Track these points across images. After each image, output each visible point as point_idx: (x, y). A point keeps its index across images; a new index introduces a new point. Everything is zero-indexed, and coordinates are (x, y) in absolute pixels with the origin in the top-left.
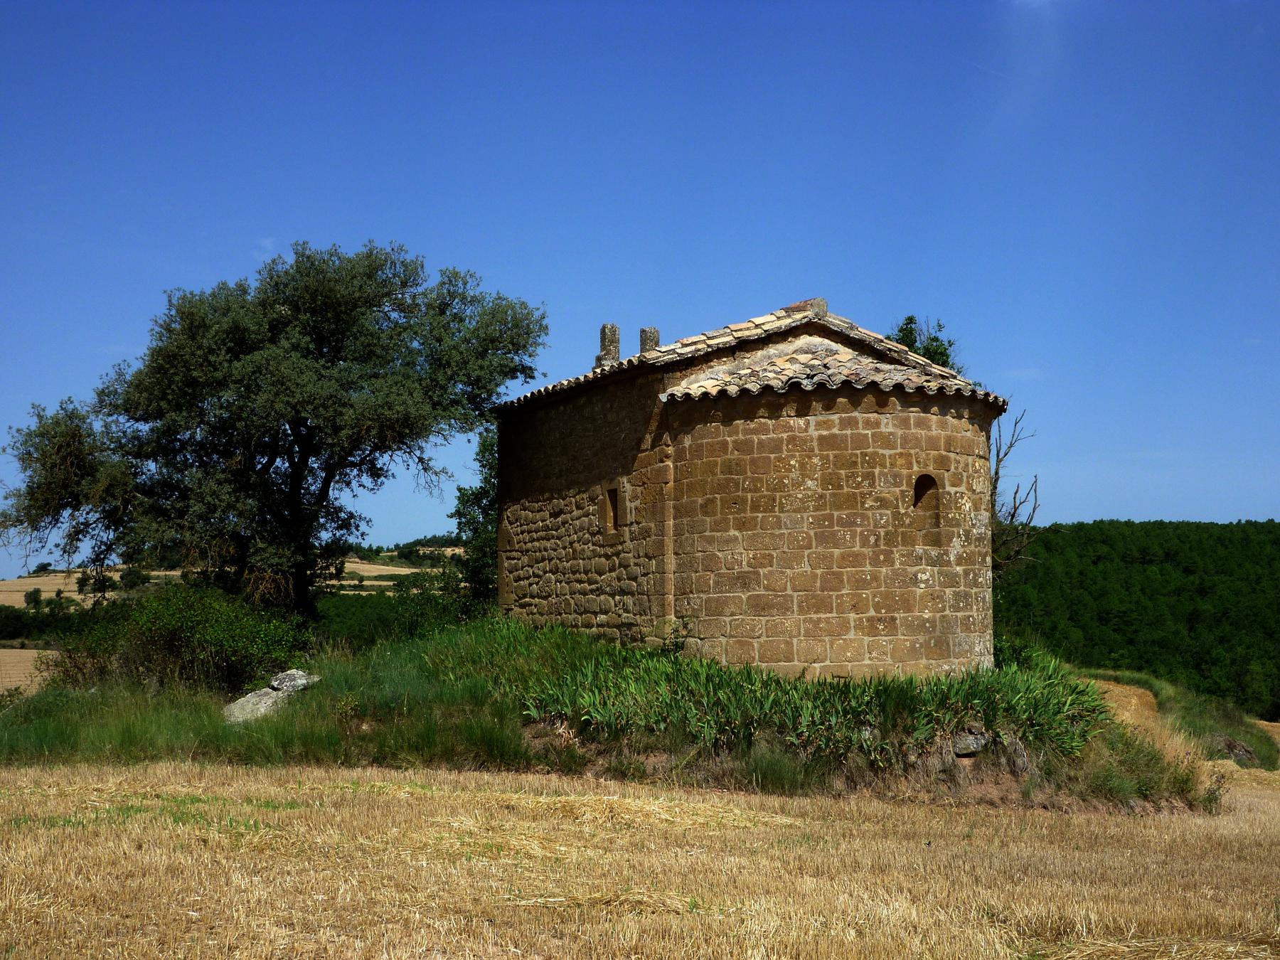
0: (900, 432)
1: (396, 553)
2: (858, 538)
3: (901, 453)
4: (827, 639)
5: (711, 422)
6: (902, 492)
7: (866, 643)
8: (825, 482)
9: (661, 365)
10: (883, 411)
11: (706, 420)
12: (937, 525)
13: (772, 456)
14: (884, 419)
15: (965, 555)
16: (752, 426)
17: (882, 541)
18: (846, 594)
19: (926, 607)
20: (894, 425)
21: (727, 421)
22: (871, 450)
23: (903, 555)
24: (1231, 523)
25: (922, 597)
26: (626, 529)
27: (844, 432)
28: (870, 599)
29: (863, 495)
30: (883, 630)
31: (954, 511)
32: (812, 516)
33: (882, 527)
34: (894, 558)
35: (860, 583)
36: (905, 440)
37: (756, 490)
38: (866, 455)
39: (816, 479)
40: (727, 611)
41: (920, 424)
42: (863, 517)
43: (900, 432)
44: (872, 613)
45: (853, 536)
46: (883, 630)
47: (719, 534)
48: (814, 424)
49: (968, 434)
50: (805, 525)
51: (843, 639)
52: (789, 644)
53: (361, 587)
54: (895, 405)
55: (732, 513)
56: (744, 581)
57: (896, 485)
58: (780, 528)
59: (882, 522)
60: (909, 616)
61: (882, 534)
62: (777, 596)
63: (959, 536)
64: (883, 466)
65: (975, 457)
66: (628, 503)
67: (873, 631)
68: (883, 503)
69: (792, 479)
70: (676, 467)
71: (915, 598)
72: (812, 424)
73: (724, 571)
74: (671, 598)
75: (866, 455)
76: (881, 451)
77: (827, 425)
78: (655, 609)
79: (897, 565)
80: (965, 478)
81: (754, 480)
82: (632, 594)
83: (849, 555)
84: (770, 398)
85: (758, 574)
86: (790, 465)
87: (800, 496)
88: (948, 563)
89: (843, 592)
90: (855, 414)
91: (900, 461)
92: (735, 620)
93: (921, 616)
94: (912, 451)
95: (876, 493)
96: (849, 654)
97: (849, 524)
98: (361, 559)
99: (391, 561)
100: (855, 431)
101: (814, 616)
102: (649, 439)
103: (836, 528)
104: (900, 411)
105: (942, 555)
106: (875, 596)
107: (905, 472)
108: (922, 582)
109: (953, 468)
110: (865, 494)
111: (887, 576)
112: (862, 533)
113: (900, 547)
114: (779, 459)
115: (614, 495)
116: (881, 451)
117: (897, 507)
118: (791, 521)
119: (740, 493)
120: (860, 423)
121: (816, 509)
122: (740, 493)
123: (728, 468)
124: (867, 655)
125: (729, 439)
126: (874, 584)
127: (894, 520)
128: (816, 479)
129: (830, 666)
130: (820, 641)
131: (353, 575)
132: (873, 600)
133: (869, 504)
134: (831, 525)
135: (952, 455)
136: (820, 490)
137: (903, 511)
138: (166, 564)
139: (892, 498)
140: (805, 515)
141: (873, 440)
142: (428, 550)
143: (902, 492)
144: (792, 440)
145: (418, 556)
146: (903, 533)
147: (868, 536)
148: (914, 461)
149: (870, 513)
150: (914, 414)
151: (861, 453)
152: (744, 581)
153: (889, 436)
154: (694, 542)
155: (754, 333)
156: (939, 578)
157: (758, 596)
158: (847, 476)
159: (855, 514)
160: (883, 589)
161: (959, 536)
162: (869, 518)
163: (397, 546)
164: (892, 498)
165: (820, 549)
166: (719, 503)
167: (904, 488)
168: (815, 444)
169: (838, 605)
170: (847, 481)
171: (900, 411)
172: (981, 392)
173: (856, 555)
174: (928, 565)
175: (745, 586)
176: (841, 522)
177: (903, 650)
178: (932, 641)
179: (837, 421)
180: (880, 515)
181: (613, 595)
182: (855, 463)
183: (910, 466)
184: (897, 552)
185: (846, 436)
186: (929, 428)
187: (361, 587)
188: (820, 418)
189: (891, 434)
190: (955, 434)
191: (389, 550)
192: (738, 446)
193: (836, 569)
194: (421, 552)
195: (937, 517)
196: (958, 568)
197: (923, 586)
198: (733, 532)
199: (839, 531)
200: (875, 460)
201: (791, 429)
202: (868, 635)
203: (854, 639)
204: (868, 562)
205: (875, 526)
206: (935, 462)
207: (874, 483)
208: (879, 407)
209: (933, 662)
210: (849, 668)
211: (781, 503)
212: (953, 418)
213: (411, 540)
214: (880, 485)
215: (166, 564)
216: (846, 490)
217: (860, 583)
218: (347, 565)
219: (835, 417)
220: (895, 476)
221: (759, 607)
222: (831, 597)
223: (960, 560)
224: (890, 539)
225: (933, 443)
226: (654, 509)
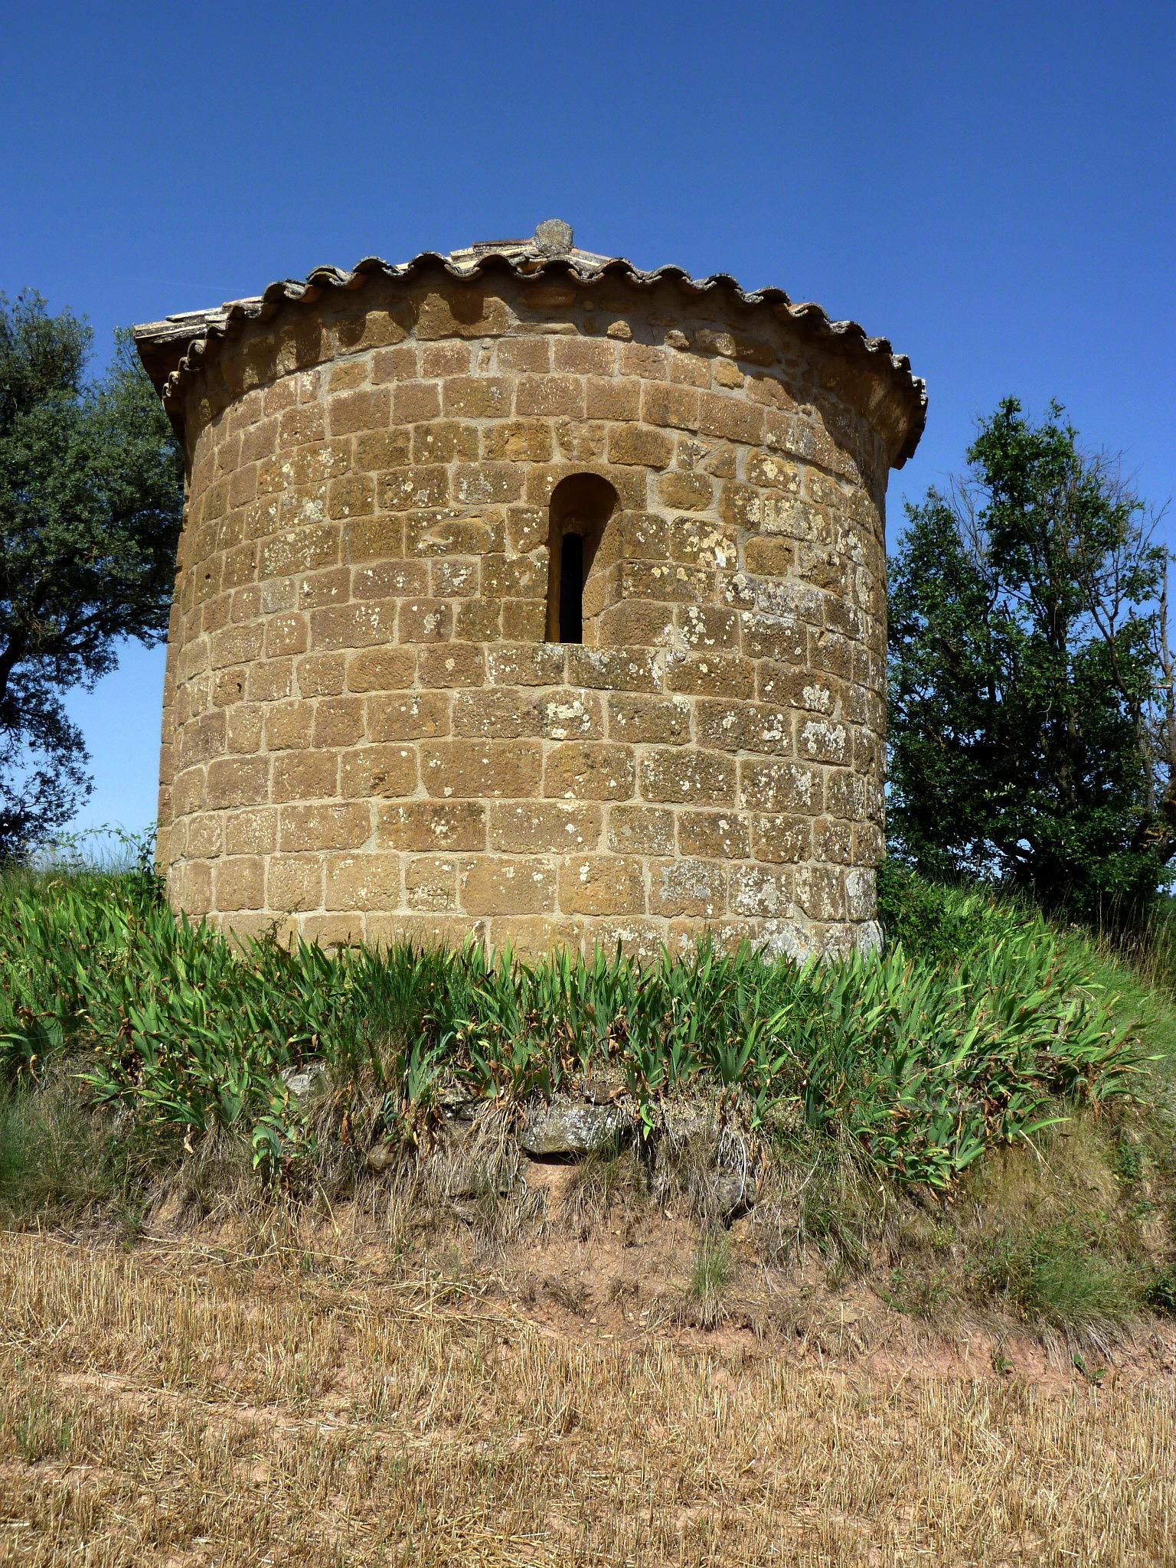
0: (516, 379)
2: (396, 622)
3: (518, 426)
4: (321, 855)
6: (515, 512)
7: (403, 867)
8: (337, 503)
9: (166, 344)
10: (472, 330)
13: (259, 463)
14: (475, 350)
15: (704, 668)
17: (455, 626)
18: (365, 751)
19: (568, 785)
20: (503, 362)
22: (440, 420)
23: (507, 660)
25: (556, 760)
27: (382, 386)
28: (419, 761)
29: (414, 523)
30: (446, 836)
31: (670, 560)
32: (309, 579)
33: (455, 594)
34: (481, 667)
36: (530, 395)
38: (428, 432)
39: (322, 498)
41: (571, 359)
42: (414, 572)
43: (516, 379)
44: (421, 795)
45: (386, 619)
46: (446, 836)
48: (328, 378)
49: (738, 394)
50: (296, 600)
51: (353, 857)
52: (257, 867)
54: (502, 314)
57: (498, 496)
59: (456, 581)
60: (518, 805)
61: (456, 609)
63: (685, 620)
64: (468, 454)
65: (764, 450)
68: (461, 539)
69: (283, 505)
71: (536, 764)
72: (326, 378)
75: (428, 432)
76: (464, 422)
79: (490, 683)
80: (718, 493)
83: (375, 661)
84: (252, 341)
86: (281, 475)
87: (291, 538)
88: (645, 682)
89: (358, 747)
90: (411, 344)
93: (553, 806)
94: (551, 422)
95: (448, 515)
96: (363, 892)
97: (379, 588)
100: (407, 383)
101: (300, 804)
103: (352, 601)
104: (518, 329)
105: (626, 663)
106: (428, 755)
107: (526, 467)
108: (556, 723)
109: (673, 463)
110: (419, 520)
111: (461, 707)
112: (405, 609)
113: (501, 641)
116: (464, 422)
117: (499, 546)
118: (273, 594)
120: (420, 364)
121: (319, 561)
124: (404, 896)
126: (429, 727)
127: (488, 577)
128: (322, 498)
129: (323, 918)
130: (308, 860)
132: (424, 766)
133: (429, 538)
134: (342, 597)
135: (674, 436)
136: (327, 521)
137: (512, 556)
139: (488, 528)
140: (297, 578)
141: (446, 397)
143: (515, 512)
146: (509, 607)
147: (421, 614)
148: (555, 442)
149: (427, 563)
151: (417, 429)
153: (489, 387)
156: (613, 718)
158: (381, 483)
159: (393, 566)
160: (450, 738)
161: (685, 620)
162: (425, 573)
164: (488, 528)
165: (319, 652)
167: (522, 503)
168: (326, 421)
169: (347, 776)
170: (382, 493)
171: (518, 329)
173: (391, 660)
174: (579, 684)
177: (495, 887)
178: (584, 869)
179: (370, 365)
180: (452, 565)
182: (402, 452)
183: (541, 453)
184: (491, 650)
185: (386, 394)
186: (602, 369)
188: (341, 364)
189: (493, 382)
190: (685, 387)
193: (347, 695)
196: (678, 698)
197: (560, 733)
199: (357, 607)
202: (409, 847)
203: (377, 858)
204: (416, 675)
205: (439, 592)
206: (616, 445)
207: (442, 494)
208: (463, 322)
209: (586, 920)
210: (363, 925)
212: (681, 349)
214: (456, 499)
216: (378, 512)
217: (397, 726)
219: (367, 358)
220: (498, 477)
222: (332, 757)
223: (683, 678)
224: (476, 622)
225: (612, 404)
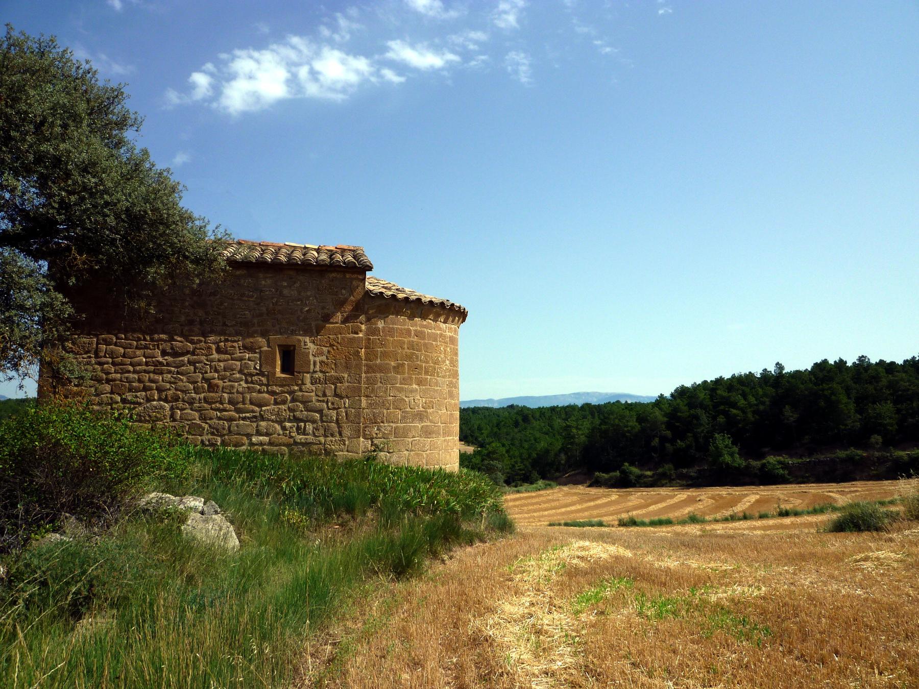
5: (401, 316)
11: (398, 313)
13: (434, 343)
16: (425, 323)
21: (411, 317)
24: (661, 396)
26: (308, 375)
37: (427, 362)
40: (410, 435)
47: (406, 386)
55: (414, 374)
58: (437, 386)
62: (435, 426)
66: (311, 358)
73: (409, 409)
81: (425, 356)
85: (426, 412)
92: (415, 440)
102: (339, 317)
119: (419, 363)
122: (419, 363)
123: (412, 346)
125: (411, 328)
154: (387, 389)
157: (427, 426)
166: (406, 367)
175: (421, 420)
198: (414, 386)
211: (438, 372)
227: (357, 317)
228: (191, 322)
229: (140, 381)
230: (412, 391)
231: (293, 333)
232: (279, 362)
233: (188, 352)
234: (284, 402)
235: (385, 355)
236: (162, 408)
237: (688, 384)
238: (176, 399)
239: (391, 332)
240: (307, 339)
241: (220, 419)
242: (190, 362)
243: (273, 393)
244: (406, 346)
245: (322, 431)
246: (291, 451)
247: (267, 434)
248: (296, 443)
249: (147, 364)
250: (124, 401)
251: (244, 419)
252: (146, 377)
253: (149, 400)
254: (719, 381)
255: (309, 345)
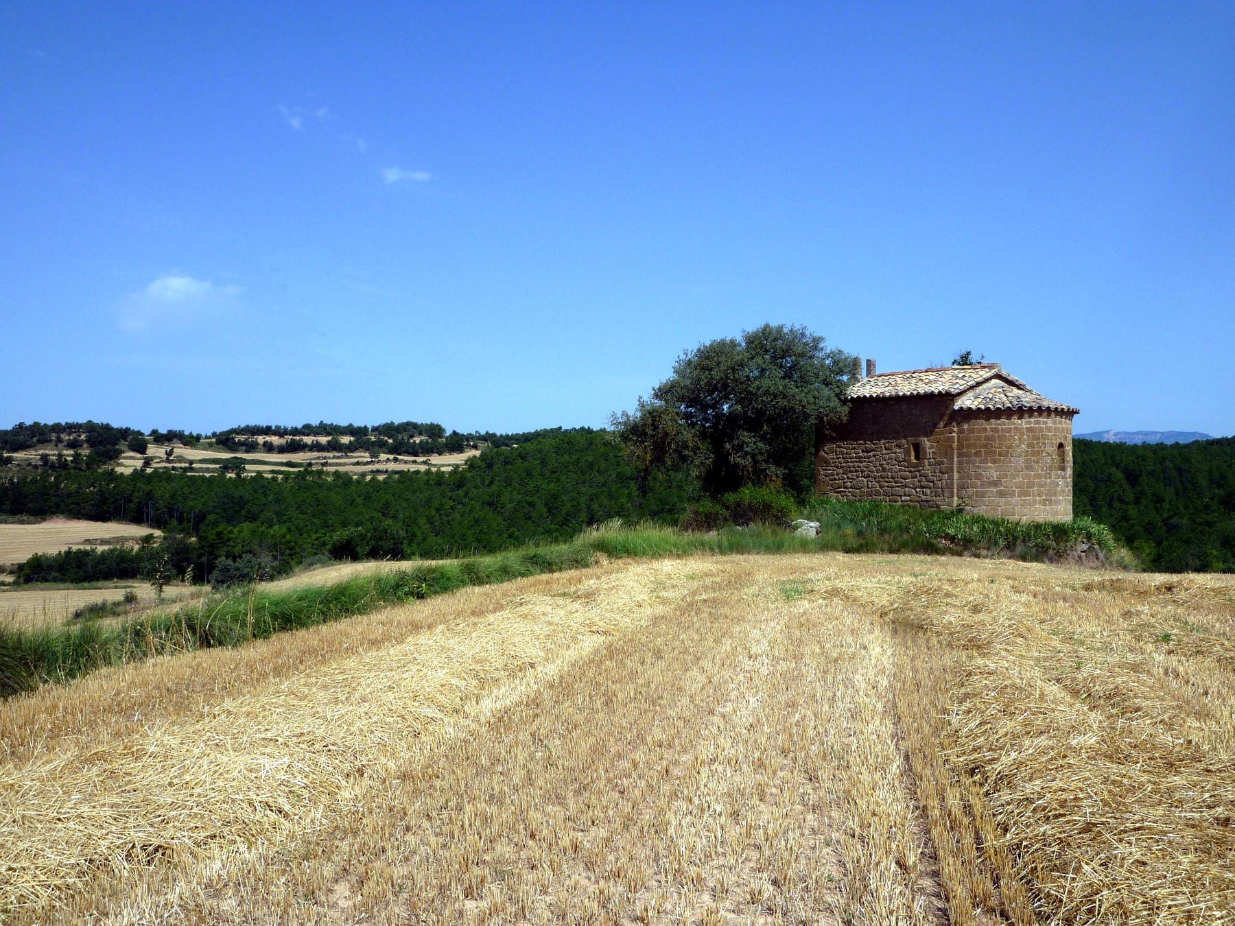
1: (214, 440)
12: (1063, 463)
21: (987, 419)
29: (1042, 451)
35: (1040, 486)
37: (1000, 448)
40: (987, 496)
41: (1060, 423)
42: (1042, 460)
43: (1053, 426)
53: (191, 469)
56: (995, 484)
66: (928, 450)
67: (1044, 504)
68: (1048, 454)
70: (958, 437)
74: (955, 490)
77: (1029, 423)
78: (946, 495)
81: (999, 444)
82: (930, 488)
91: (1054, 437)
98: (185, 444)
99: (210, 446)
102: (942, 424)
114: (1010, 436)
115: (917, 448)
123: (988, 438)
131: (181, 459)
138: (8, 447)
142: (242, 438)
144: (1015, 428)
145: (234, 442)
150: (1058, 418)
152: (995, 484)
155: (980, 379)
163: (214, 434)
172: (1066, 408)
173: (1040, 474)
176: (1034, 462)
181: (915, 488)
187: (191, 469)
191: (207, 437)
192: (992, 430)
194: (237, 440)
195: (1063, 459)
198: (989, 464)
200: (1046, 437)
201: (1015, 424)
213: (226, 428)
215: (8, 447)
217: (1040, 486)
218: (175, 450)
219: (1032, 420)
221: (1002, 494)
226: (948, 453)
227: (951, 423)
228: (873, 433)
229: (854, 467)
230: (988, 468)
231: (919, 436)
232: (913, 453)
233: (872, 450)
234: (916, 477)
235: (968, 446)
236: (863, 481)
237: (42, 422)
238: (869, 476)
239: (971, 431)
240: (925, 439)
241: (888, 487)
242: (874, 456)
243: (910, 472)
244: (983, 439)
245: (934, 494)
246: (920, 505)
247: (909, 496)
248: (922, 501)
249: (856, 457)
250: (848, 478)
251: (898, 487)
252: (856, 464)
253: (858, 477)
254: (507, 436)
255: (926, 442)
